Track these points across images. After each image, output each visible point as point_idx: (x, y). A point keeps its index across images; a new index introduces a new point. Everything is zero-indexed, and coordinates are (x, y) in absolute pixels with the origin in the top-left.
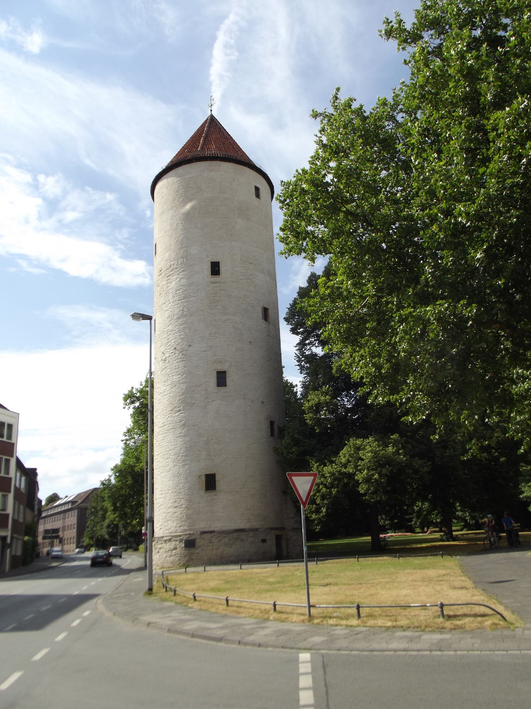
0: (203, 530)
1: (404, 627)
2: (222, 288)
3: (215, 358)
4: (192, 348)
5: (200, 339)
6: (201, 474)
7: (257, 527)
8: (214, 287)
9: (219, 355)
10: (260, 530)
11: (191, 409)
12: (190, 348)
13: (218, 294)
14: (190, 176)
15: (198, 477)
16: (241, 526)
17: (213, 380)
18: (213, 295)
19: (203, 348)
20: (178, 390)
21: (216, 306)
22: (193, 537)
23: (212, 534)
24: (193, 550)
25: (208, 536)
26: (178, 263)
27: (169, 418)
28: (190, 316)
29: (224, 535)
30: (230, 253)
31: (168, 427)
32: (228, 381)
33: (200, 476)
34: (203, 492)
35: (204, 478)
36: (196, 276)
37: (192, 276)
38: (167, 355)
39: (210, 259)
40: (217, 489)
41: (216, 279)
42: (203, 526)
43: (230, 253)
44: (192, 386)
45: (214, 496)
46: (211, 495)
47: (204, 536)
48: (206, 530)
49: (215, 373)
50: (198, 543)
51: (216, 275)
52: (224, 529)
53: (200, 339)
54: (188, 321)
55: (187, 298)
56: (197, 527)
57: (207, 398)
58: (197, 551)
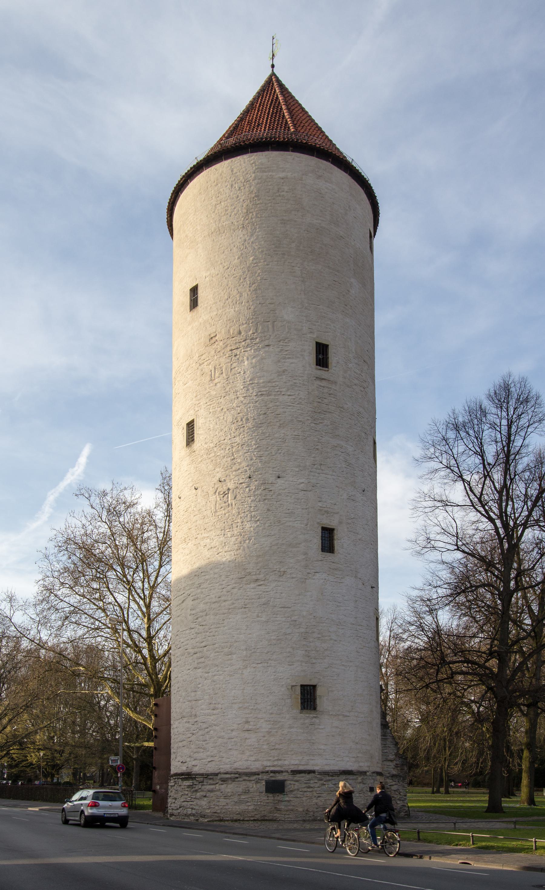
0: (296, 768)
1: (487, 404)
2: (331, 392)
3: (320, 504)
4: (283, 482)
5: (297, 470)
6: (294, 684)
7: (365, 769)
8: (321, 386)
9: (325, 502)
10: (368, 774)
11: (279, 581)
12: (278, 480)
13: (326, 401)
14: (282, 175)
15: (290, 687)
16: (364, 766)
17: (317, 541)
18: (319, 400)
19: (302, 485)
20: (255, 546)
21: (323, 419)
22: (279, 777)
23: (312, 775)
24: (280, 797)
25: (303, 778)
26: (256, 331)
27: (236, 590)
28: (280, 427)
29: (328, 778)
30: (343, 334)
31: (233, 604)
32: (337, 544)
33: (292, 686)
34: (296, 711)
35: (298, 690)
36: (291, 361)
37: (285, 358)
38: (231, 485)
39: (315, 336)
40: (318, 708)
41: (322, 373)
42: (297, 762)
43: (343, 334)
44: (283, 544)
45: (314, 719)
46: (307, 717)
47: (298, 777)
48: (301, 768)
49: (320, 529)
50: (290, 785)
51: (323, 367)
52: (327, 768)
53: (297, 470)
54: (276, 436)
55: (275, 395)
56: (286, 762)
57: (306, 567)
58: (287, 799)
